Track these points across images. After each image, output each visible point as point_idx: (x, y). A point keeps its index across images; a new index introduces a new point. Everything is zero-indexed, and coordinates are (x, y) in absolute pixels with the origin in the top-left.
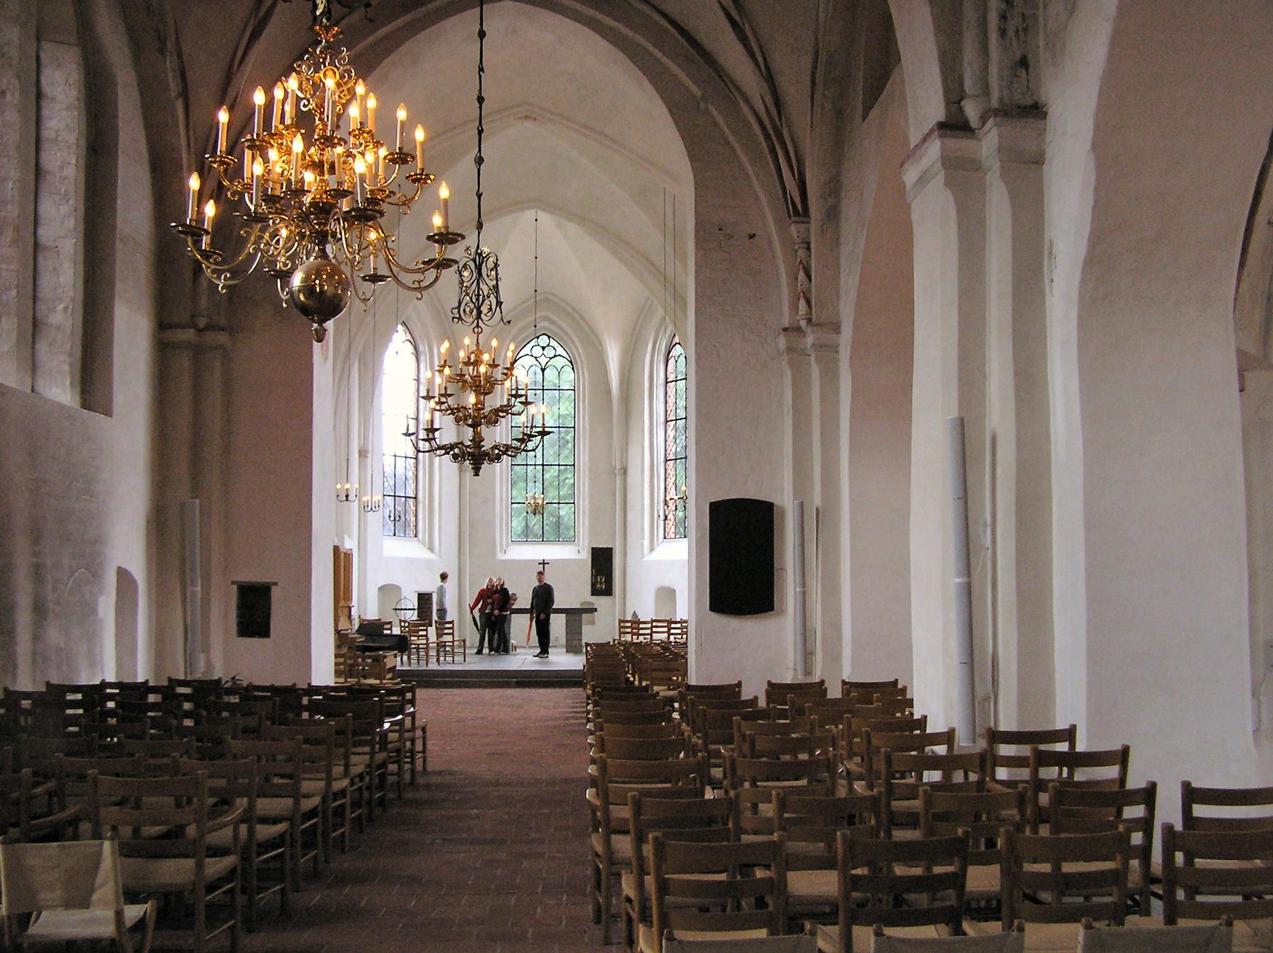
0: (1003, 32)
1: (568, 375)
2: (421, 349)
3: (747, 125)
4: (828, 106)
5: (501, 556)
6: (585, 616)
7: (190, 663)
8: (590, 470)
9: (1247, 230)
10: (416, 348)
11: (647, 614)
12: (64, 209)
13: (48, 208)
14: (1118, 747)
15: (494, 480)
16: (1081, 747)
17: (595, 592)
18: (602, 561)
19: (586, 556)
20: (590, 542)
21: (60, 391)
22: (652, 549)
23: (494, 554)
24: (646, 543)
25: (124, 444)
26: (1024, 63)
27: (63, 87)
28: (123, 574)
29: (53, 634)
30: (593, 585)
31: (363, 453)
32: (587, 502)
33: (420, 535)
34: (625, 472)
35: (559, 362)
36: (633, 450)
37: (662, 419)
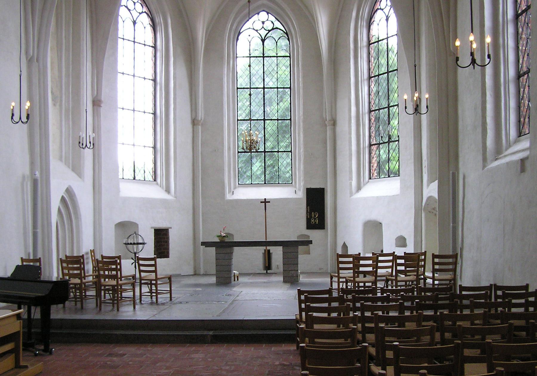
1: (284, 42)
2: (157, 20)
5: (229, 197)
6: (301, 248)
8: (304, 122)
10: (152, 20)
11: (356, 247)
15: (222, 131)
17: (310, 226)
18: (316, 200)
19: (301, 195)
20: (306, 181)
22: (359, 188)
23: (223, 194)
24: (354, 183)
30: (308, 220)
31: (97, 103)
32: (302, 150)
33: (159, 180)
34: (334, 123)
35: (276, 34)
36: (341, 104)
37: (366, 76)
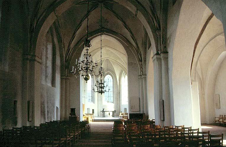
0: (163, 43)
3: (134, 50)
4: (144, 48)
7: (57, 120)
9: (162, 86)
12: (50, 62)
13: (48, 61)
14: (198, 128)
16: (192, 129)
21: (50, 85)
25: (57, 90)
26: (165, 47)
27: (50, 47)
28: (57, 107)
29: (49, 115)
